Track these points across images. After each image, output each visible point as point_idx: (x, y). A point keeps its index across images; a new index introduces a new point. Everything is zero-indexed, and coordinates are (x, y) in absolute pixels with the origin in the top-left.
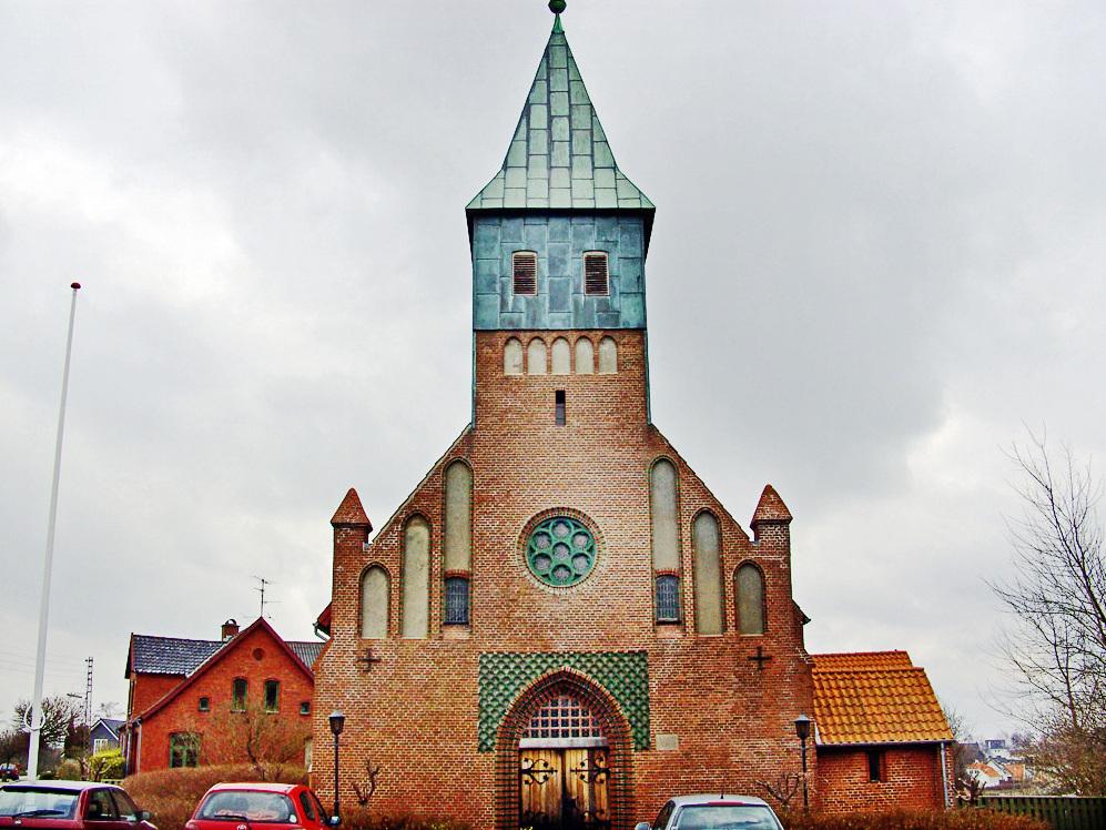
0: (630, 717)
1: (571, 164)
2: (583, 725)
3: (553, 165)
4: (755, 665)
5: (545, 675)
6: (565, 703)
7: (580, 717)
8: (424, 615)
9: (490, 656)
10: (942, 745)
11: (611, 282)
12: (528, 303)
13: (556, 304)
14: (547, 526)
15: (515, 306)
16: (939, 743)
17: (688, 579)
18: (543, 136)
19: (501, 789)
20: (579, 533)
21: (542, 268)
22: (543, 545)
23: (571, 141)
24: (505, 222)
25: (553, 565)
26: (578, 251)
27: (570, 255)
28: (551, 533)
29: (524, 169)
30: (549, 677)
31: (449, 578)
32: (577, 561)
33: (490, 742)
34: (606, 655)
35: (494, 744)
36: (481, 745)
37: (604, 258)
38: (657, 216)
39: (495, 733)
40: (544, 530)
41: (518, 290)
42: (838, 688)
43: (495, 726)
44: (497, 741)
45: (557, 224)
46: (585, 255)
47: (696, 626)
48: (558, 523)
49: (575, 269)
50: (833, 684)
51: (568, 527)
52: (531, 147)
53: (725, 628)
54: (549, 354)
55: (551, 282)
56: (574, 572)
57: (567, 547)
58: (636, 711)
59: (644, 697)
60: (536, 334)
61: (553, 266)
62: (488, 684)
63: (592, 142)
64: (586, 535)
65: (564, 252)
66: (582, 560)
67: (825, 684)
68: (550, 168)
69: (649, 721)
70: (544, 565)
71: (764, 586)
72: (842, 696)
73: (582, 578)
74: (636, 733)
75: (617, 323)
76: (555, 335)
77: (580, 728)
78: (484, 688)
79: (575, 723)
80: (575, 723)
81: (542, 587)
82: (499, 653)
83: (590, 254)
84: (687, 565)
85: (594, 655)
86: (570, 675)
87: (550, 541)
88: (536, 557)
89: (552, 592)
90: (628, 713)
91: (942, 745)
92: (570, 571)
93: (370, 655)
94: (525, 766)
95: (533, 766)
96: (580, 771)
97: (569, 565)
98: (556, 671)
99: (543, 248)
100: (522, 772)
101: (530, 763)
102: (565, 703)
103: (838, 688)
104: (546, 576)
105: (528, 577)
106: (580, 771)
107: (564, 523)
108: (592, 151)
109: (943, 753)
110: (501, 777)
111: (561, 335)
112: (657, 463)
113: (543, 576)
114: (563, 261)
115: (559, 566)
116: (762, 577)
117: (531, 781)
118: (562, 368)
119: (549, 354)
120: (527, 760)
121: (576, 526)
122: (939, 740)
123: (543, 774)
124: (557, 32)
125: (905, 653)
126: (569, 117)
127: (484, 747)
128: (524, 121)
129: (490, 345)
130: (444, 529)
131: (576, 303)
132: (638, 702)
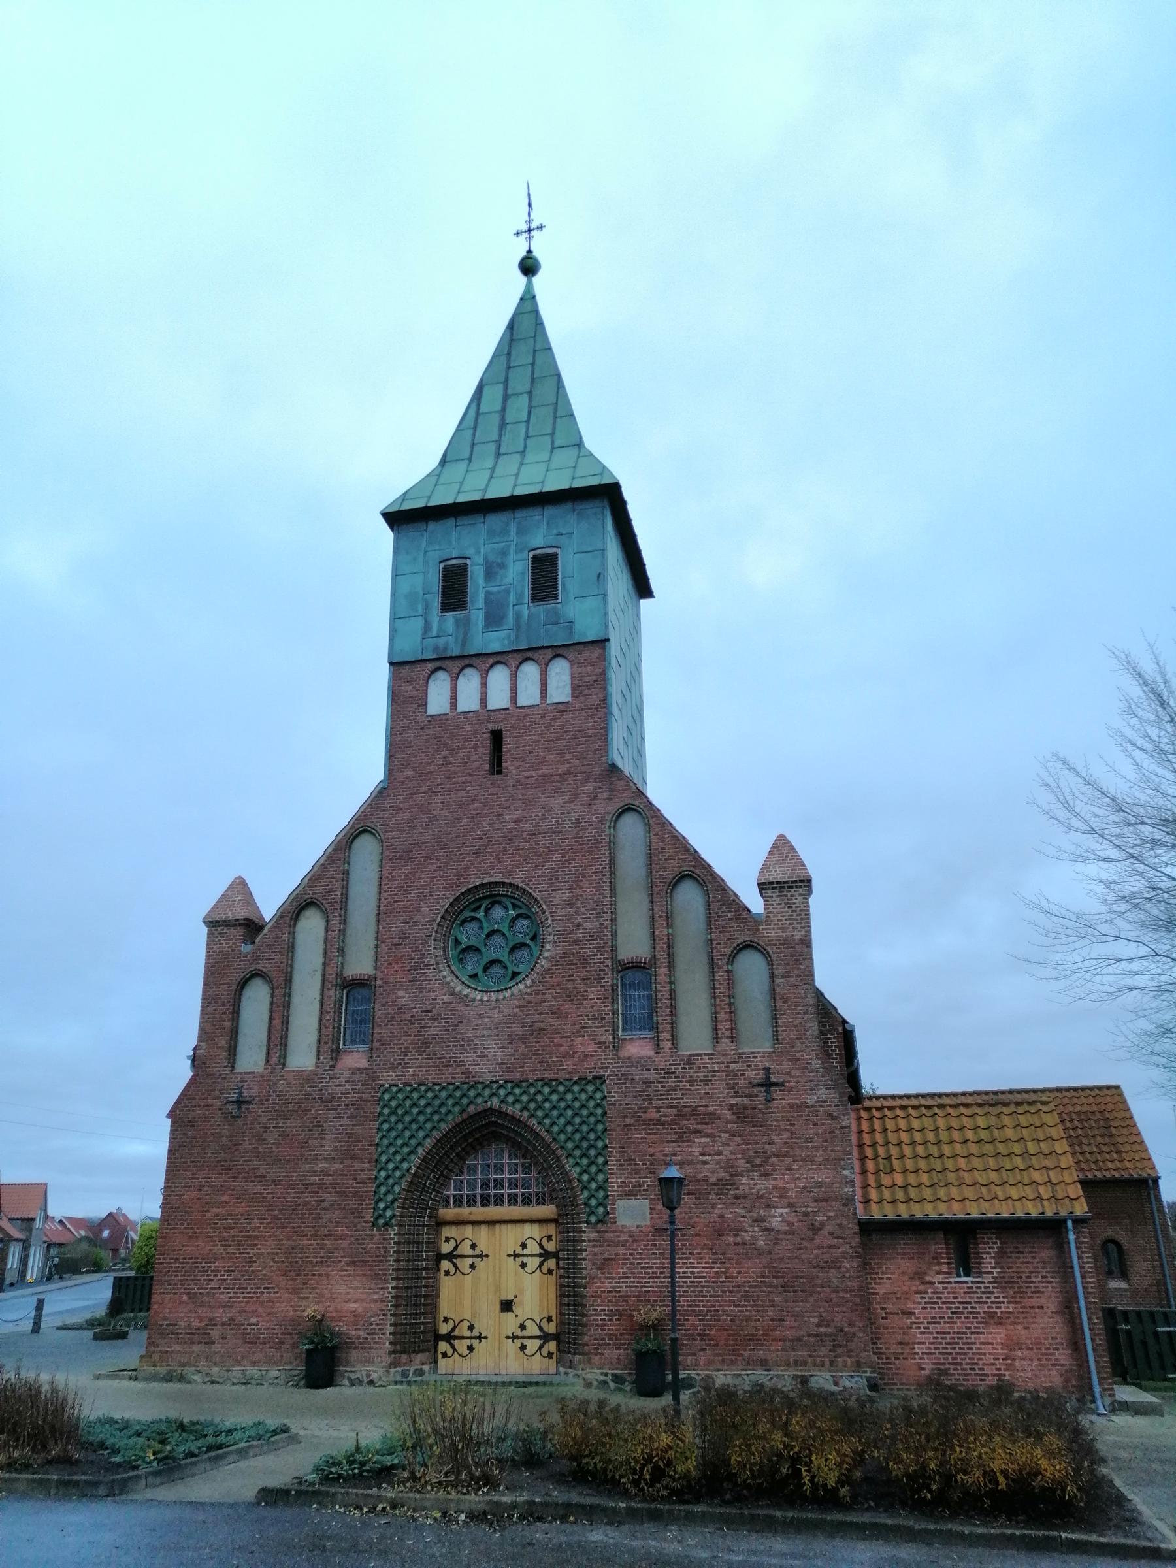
0: (581, 1174)
1: (525, 447)
2: (510, 1188)
3: (576, 476)
4: (776, 1093)
5: (465, 1115)
6: (499, 1155)
7: (520, 1175)
8: (313, 1038)
9: (394, 1089)
10: (1070, 1224)
11: (563, 585)
12: (457, 622)
13: (494, 619)
14: (478, 908)
15: (440, 629)
16: (1064, 1221)
17: (663, 970)
18: (495, 420)
19: (401, 1283)
20: (519, 916)
21: (476, 574)
22: (468, 934)
23: (528, 421)
24: (432, 526)
25: (485, 961)
26: (522, 551)
27: (512, 556)
28: (483, 919)
29: (467, 461)
30: (471, 1117)
31: (355, 986)
32: (518, 954)
33: (389, 1213)
34: (547, 1083)
35: (393, 1216)
36: (377, 1219)
37: (555, 555)
38: (622, 484)
39: (395, 1200)
40: (473, 914)
41: (446, 607)
42: (910, 1130)
43: (397, 1189)
44: (398, 1211)
45: (495, 520)
46: (531, 554)
47: (674, 1040)
48: (493, 904)
49: (518, 573)
50: (902, 1124)
51: (506, 908)
52: (477, 434)
53: (716, 1039)
54: (484, 685)
55: (488, 594)
56: (512, 968)
57: (504, 934)
58: (589, 1165)
59: (600, 1144)
60: (467, 661)
61: (489, 574)
62: (389, 1130)
63: (555, 418)
64: (527, 917)
65: (504, 553)
66: (524, 953)
67: (877, 1125)
68: (498, 455)
69: (607, 1180)
70: (473, 964)
71: (772, 976)
72: (913, 1143)
73: (520, 978)
74: (589, 1199)
75: (571, 634)
76: (491, 661)
77: (506, 1191)
78: (384, 1136)
79: (513, 1184)
80: (513, 1184)
81: (466, 991)
82: (406, 1085)
83: (538, 552)
84: (662, 955)
85: (532, 1084)
86: (500, 1113)
87: (482, 928)
88: (464, 950)
89: (479, 997)
90: (578, 1169)
91: (1070, 1224)
92: (505, 967)
93: (240, 1094)
94: (446, 1248)
95: (456, 1248)
96: (477, 1256)
97: (505, 959)
98: (480, 1109)
99: (478, 552)
100: (440, 1257)
101: (453, 1243)
102: (499, 1155)
103: (910, 1130)
104: (474, 976)
105: (448, 979)
106: (477, 1256)
107: (499, 903)
108: (554, 428)
109: (1072, 1237)
110: (402, 1265)
111: (498, 658)
112: (620, 815)
113: (471, 976)
114: (502, 566)
115: (493, 962)
116: (770, 964)
117: (452, 1270)
118: (499, 698)
119: (484, 685)
120: (447, 1240)
121: (515, 906)
122: (1063, 1214)
123: (526, 1251)
124: (528, 301)
125: (1117, 1087)
126: (530, 393)
127: (381, 1222)
128: (474, 406)
129: (410, 681)
130: (344, 921)
131: (518, 616)
132: (592, 1152)
